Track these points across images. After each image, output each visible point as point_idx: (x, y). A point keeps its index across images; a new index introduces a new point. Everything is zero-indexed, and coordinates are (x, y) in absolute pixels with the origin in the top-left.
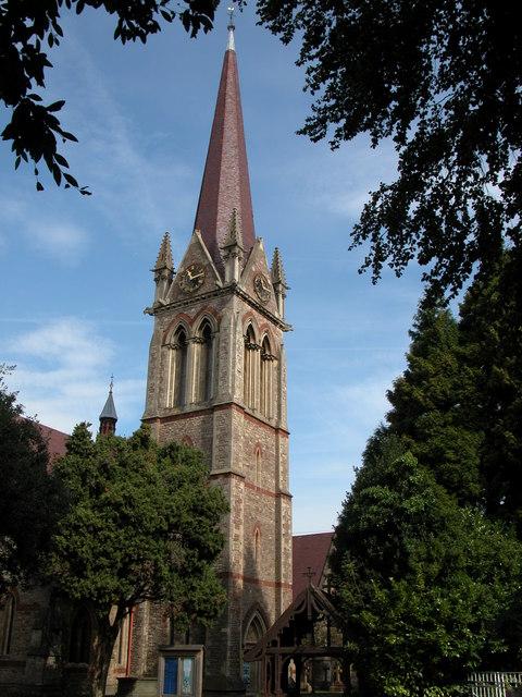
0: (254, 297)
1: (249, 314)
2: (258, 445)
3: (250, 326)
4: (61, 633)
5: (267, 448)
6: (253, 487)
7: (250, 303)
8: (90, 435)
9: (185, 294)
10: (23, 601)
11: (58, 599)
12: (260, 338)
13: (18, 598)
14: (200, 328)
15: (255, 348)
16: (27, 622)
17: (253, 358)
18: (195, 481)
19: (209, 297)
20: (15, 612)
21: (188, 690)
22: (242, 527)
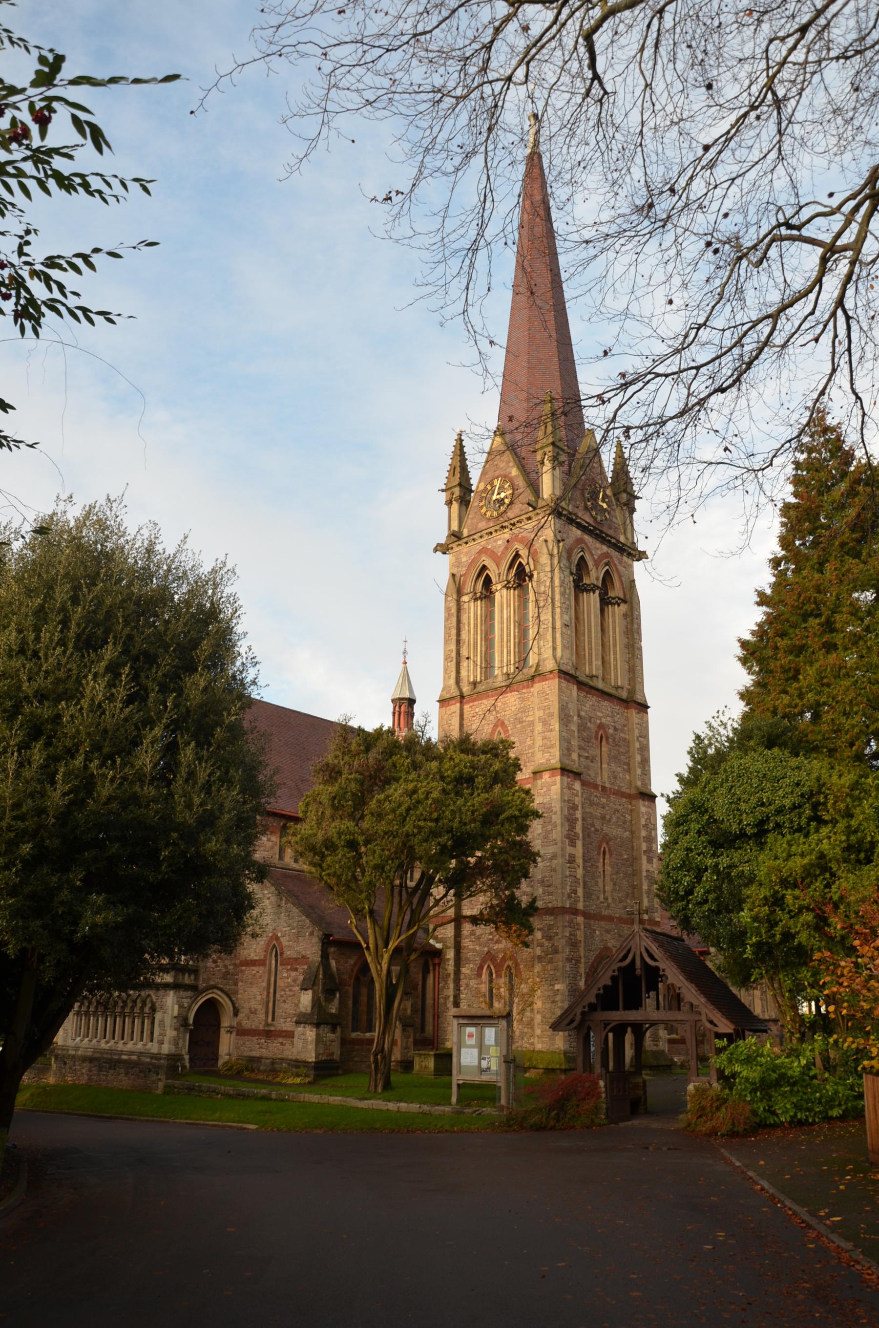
0: (586, 518)
1: (579, 541)
2: (601, 726)
5: (616, 729)
6: (596, 786)
7: (579, 526)
10: (288, 953)
11: (332, 949)
12: (594, 576)
13: (282, 949)
15: (591, 589)
16: (295, 981)
20: (279, 968)
22: (579, 844)
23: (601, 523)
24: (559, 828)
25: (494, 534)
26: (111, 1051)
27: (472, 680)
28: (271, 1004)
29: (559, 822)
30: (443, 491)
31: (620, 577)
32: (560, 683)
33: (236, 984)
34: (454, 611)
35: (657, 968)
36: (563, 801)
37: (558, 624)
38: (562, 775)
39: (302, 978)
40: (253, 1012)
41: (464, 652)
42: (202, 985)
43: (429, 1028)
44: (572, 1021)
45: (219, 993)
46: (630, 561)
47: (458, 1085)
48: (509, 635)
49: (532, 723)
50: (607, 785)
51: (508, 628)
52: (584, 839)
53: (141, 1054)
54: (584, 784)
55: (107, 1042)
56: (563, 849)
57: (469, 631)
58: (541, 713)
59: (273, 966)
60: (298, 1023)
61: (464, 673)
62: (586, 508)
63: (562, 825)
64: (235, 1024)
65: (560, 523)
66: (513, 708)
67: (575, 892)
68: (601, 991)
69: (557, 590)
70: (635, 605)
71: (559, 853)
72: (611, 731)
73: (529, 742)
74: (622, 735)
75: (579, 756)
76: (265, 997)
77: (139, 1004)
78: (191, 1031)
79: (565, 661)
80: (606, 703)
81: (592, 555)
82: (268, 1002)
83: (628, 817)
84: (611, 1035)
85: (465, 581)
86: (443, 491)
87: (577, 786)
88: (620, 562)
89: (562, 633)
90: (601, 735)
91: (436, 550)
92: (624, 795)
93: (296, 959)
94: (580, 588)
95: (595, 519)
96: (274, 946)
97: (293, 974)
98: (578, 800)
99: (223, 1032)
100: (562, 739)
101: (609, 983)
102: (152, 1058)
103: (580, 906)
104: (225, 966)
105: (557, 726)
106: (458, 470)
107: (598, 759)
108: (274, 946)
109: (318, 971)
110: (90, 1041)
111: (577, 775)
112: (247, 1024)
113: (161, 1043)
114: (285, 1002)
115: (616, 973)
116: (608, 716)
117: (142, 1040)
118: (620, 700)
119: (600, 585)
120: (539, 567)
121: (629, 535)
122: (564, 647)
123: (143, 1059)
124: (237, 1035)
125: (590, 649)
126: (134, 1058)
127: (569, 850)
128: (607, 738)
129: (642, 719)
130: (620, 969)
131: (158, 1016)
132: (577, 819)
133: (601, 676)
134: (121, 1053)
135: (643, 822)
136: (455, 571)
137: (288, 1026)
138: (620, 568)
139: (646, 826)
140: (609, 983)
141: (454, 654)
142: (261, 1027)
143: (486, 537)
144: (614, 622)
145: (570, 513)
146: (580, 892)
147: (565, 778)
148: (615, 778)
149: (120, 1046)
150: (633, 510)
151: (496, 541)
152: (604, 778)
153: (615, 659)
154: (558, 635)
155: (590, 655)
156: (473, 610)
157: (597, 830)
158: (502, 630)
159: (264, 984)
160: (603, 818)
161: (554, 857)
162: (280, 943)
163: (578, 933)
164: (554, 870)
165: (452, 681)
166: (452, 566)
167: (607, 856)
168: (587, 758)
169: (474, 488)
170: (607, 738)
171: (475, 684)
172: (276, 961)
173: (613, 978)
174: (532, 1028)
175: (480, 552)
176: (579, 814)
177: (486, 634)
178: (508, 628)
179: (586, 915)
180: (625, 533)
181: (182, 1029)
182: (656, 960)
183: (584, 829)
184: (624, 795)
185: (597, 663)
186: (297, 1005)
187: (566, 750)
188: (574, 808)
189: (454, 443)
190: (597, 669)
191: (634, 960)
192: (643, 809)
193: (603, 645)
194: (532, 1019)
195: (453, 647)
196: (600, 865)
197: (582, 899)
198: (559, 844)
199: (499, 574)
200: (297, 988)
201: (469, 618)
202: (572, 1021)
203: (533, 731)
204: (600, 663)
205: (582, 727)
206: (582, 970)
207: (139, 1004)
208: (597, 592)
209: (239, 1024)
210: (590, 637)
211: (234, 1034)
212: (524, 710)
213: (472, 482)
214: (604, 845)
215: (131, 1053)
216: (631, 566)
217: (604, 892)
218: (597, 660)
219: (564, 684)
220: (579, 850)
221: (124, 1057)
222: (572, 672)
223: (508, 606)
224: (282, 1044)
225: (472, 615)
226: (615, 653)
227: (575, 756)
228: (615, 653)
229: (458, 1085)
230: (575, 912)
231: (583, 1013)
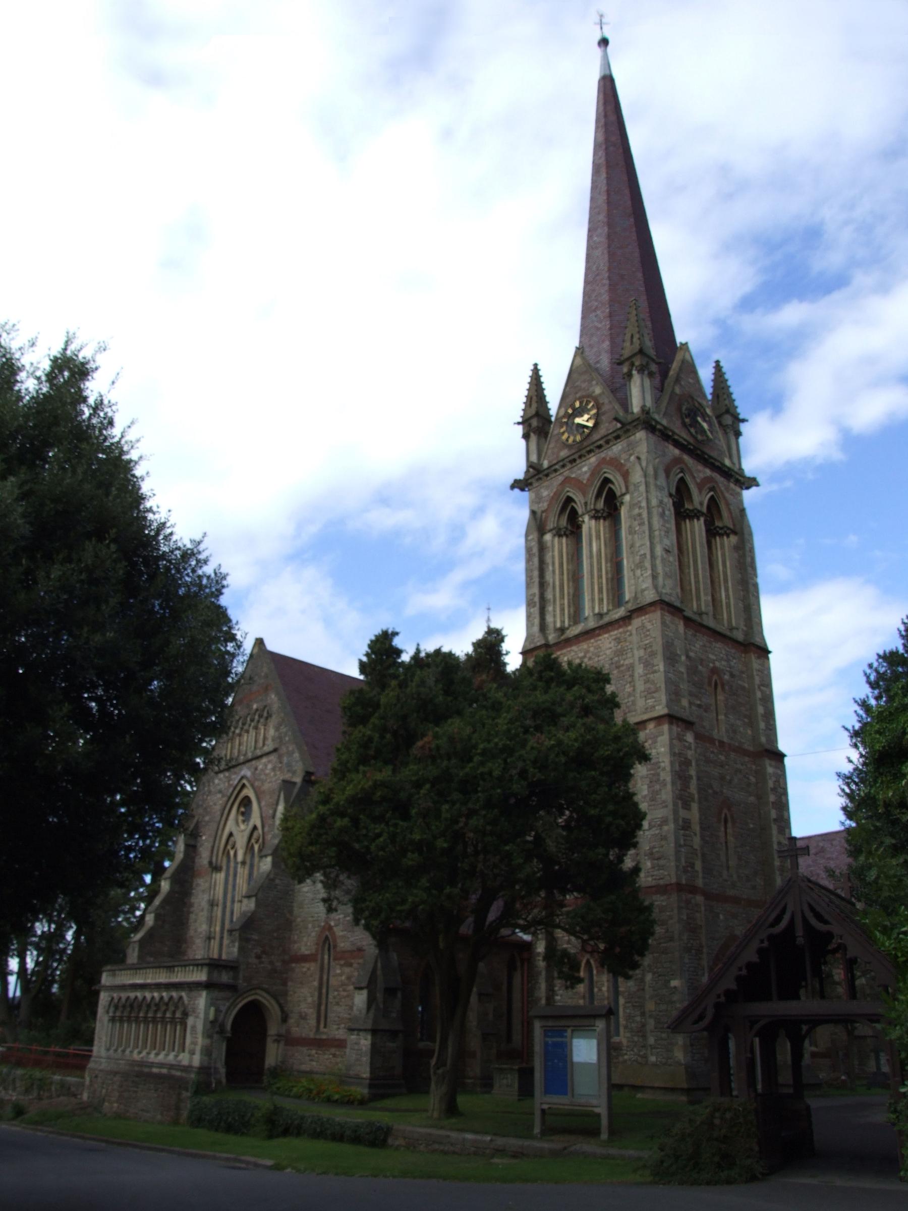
0: (683, 435)
1: (677, 461)
2: (714, 671)
3: (682, 481)
4: (399, 995)
5: (732, 675)
6: (711, 740)
7: (677, 444)
8: (398, 652)
9: (570, 447)
10: (342, 945)
14: (598, 495)
15: (694, 515)
16: (349, 978)
17: (693, 533)
18: (586, 711)
19: (607, 442)
20: (332, 963)
21: (840, 990)
22: (695, 807)
23: (701, 442)
24: (669, 787)
25: (578, 462)
26: (142, 1064)
27: (558, 625)
28: (323, 1007)
29: (669, 779)
30: (519, 423)
31: (728, 504)
32: (662, 615)
33: (285, 984)
34: (535, 550)
35: (830, 936)
36: (673, 754)
37: (659, 550)
38: (671, 723)
39: (356, 974)
40: (303, 1017)
41: (549, 595)
42: (241, 983)
43: (517, 1037)
44: (701, 1017)
45: (265, 995)
46: (738, 489)
47: (543, 1111)
48: (600, 570)
49: (631, 667)
50: (725, 740)
51: (599, 563)
52: (700, 803)
53: (171, 1067)
54: (698, 737)
55: (140, 1053)
56: (676, 812)
57: (554, 571)
58: (642, 653)
59: (326, 961)
60: (351, 1030)
61: (549, 619)
62: (684, 424)
63: (673, 783)
64: (283, 1031)
65: (653, 438)
66: (608, 652)
67: (692, 865)
68: (744, 972)
69: (655, 512)
70: (746, 536)
71: (671, 817)
72: (727, 677)
73: (628, 689)
74: (740, 682)
75: (690, 703)
76: (316, 998)
77: (172, 1008)
78: (229, 1041)
79: (667, 590)
80: (719, 645)
81: (694, 477)
82: (320, 1005)
83: (753, 779)
84: (757, 1040)
85: (546, 517)
86: (519, 423)
87: (690, 737)
88: (727, 489)
89: (663, 560)
90: (714, 681)
91: (513, 487)
92: (746, 753)
93: (351, 952)
94: (682, 514)
95: (696, 438)
96: (327, 938)
97: (347, 970)
98: (690, 754)
99: (269, 1040)
100: (668, 681)
101: (755, 958)
102: (170, 1069)
103: (700, 882)
104: (271, 963)
105: (661, 667)
106: (534, 398)
107: (713, 708)
108: (327, 938)
109: (376, 962)
110: (167, 1055)
111: (688, 724)
112: (296, 1031)
113: (192, 1053)
114: (337, 1004)
115: (766, 944)
116: (722, 659)
117: (173, 1050)
118: (735, 642)
119: (704, 510)
120: (631, 488)
121: (735, 460)
122: (667, 576)
123: (174, 1072)
124: (286, 1044)
125: (697, 582)
126: (164, 1071)
127: (683, 813)
128: (723, 685)
129: (763, 665)
130: (771, 938)
131: (190, 1021)
132: (691, 777)
133: (711, 613)
134: (152, 1065)
135: (771, 784)
136: (535, 508)
137: (339, 1033)
138: (727, 495)
139: (774, 790)
140: (755, 958)
141: (537, 599)
142: (312, 1035)
143: (569, 466)
144: (723, 555)
145: (665, 428)
146: (698, 865)
147: (674, 728)
148: (735, 732)
149: (152, 1057)
150: (738, 434)
151: (580, 468)
152: (721, 733)
153: (727, 597)
154: (658, 562)
155: (698, 589)
156: (557, 546)
157: (715, 793)
158: (592, 566)
159: (316, 984)
160: (722, 778)
161: (664, 821)
162: (334, 934)
163: (698, 915)
164: (664, 838)
165: (536, 629)
166: (532, 502)
167: (729, 825)
168: (699, 706)
169: (553, 419)
170: (723, 685)
171: (562, 630)
172: (329, 956)
173: (760, 951)
174: (644, 1037)
175: (563, 483)
176: (693, 772)
177: (574, 575)
178: (599, 563)
179: (708, 896)
180: (731, 457)
181: (216, 1036)
182: (826, 922)
183: (700, 790)
184: (746, 753)
185: (705, 598)
186: (351, 1008)
187: (674, 694)
188: (686, 763)
189: (530, 373)
190: (707, 605)
191: (792, 922)
192: (770, 770)
193: (712, 582)
194: (644, 1025)
195: (536, 590)
196: (722, 834)
197: (701, 875)
198: (671, 806)
199: (586, 503)
200: (351, 987)
201: (553, 557)
202: (701, 1017)
203: (632, 676)
204: (710, 598)
205: (692, 670)
206: (705, 963)
207: (172, 1008)
208: (702, 519)
209: (288, 1031)
210: (696, 570)
211: (282, 1043)
212: (620, 653)
213: (549, 406)
214: (725, 811)
215: (161, 1065)
216: (740, 495)
217: (728, 867)
218: (706, 594)
219: (668, 618)
220: (694, 814)
221: (155, 1070)
222: (677, 604)
223: (598, 537)
224: (334, 1055)
225: (556, 553)
226: (727, 590)
227: (685, 702)
228: (727, 590)
229: (543, 1111)
230: (693, 890)
231: (717, 1006)
